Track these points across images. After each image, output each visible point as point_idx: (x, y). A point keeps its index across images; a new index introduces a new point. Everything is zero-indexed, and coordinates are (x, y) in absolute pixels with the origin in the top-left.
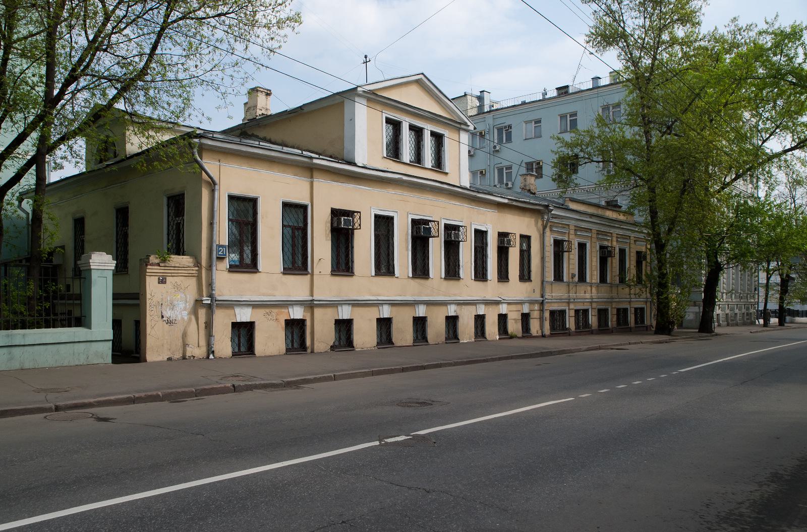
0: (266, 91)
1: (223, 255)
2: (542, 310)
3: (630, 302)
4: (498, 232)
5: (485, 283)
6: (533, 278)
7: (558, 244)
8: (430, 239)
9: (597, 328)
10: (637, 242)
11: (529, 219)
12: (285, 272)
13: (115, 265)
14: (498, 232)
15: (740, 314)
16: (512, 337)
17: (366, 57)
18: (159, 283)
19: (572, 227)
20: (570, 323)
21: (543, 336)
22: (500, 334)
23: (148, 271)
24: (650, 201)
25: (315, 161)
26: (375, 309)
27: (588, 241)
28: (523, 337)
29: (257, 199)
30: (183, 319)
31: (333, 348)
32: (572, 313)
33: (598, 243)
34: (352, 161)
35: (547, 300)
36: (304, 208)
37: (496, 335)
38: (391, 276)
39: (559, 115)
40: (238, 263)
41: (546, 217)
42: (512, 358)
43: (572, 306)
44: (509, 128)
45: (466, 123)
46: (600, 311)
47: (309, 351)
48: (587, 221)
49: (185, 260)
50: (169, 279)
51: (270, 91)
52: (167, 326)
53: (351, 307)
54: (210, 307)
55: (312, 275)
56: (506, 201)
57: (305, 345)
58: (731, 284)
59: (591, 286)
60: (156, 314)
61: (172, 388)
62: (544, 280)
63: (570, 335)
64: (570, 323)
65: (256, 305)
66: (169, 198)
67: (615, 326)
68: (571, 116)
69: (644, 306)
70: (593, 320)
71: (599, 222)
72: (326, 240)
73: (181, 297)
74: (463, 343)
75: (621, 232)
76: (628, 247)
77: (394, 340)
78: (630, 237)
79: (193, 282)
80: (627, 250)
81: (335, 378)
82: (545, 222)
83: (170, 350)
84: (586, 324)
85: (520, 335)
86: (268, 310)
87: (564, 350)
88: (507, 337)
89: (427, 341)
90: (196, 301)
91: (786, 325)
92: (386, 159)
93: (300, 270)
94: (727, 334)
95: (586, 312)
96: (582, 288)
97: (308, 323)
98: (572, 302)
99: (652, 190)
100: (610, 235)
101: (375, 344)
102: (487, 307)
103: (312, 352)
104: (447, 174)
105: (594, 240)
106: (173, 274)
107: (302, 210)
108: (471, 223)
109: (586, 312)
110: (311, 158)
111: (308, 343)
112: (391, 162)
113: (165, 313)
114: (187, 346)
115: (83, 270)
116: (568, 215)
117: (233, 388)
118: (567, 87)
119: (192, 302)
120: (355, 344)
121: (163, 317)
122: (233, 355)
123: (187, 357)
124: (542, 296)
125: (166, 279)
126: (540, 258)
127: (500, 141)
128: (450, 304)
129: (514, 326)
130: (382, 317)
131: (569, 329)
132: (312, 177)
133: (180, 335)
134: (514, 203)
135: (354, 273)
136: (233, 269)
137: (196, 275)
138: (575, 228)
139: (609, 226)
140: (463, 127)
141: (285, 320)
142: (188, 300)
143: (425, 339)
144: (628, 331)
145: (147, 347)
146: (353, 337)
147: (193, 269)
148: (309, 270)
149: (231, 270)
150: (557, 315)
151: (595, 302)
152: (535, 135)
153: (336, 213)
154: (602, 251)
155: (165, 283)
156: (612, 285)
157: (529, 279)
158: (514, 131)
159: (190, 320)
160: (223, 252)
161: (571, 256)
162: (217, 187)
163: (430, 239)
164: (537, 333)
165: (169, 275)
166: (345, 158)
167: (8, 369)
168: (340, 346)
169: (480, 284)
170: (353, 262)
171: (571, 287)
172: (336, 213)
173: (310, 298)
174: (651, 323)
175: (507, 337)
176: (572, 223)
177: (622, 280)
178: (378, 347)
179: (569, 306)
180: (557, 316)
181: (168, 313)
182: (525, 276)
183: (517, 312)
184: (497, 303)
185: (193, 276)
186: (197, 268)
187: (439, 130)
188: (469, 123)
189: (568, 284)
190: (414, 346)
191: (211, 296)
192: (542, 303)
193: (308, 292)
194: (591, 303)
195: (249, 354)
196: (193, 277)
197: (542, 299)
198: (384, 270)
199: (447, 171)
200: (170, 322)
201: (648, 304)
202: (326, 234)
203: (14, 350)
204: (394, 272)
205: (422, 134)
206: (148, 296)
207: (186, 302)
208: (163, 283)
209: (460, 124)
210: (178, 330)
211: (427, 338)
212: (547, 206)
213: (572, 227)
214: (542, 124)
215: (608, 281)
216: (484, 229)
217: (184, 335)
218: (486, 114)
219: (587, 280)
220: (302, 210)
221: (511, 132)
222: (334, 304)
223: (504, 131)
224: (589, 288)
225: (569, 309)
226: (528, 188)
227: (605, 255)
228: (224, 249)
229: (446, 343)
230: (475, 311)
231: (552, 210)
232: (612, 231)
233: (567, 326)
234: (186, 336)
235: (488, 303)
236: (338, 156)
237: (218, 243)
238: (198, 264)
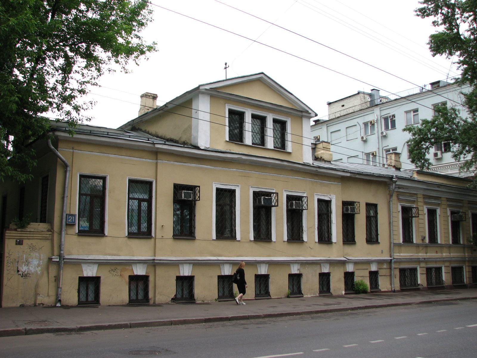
0: (153, 95)
1: (72, 222)
5: (330, 246)
7: (406, 211)
12: (129, 236)
17: (226, 64)
18: (16, 244)
20: (421, 279)
22: (345, 290)
23: (6, 234)
25: (157, 146)
31: (174, 300)
34: (196, 145)
35: (395, 260)
36: (150, 184)
37: (342, 290)
38: (352, 244)
40: (87, 229)
44: (393, 117)
46: (453, 269)
48: (430, 190)
49: (42, 226)
50: (25, 242)
51: (156, 95)
52: (22, 278)
57: (149, 297)
60: (12, 269)
64: (421, 279)
65: (101, 264)
70: (446, 277)
73: (35, 256)
79: (47, 244)
86: (113, 267)
92: (228, 143)
101: (217, 297)
107: (148, 186)
111: (151, 295)
113: (20, 268)
114: (38, 295)
118: (438, 82)
120: (196, 297)
123: (37, 304)
125: (22, 241)
127: (387, 128)
135: (195, 237)
136: (82, 233)
137: (50, 238)
139: (464, 194)
140: (304, 114)
141: (129, 276)
142: (42, 258)
143: (267, 293)
147: (47, 233)
148: (153, 235)
149: (80, 234)
150: (407, 273)
152: (414, 123)
153: (178, 188)
154: (454, 216)
155: (22, 244)
157: (377, 242)
158: (397, 119)
159: (42, 273)
160: (72, 220)
162: (68, 169)
163: (272, 208)
165: (25, 238)
168: (182, 298)
172: (178, 188)
178: (219, 300)
180: (407, 273)
181: (24, 269)
183: (448, 274)
185: (48, 239)
186: (50, 233)
190: (256, 299)
191: (60, 256)
193: (389, 255)
196: (47, 240)
197: (391, 258)
198: (227, 233)
200: (25, 276)
206: (6, 254)
208: (20, 245)
209: (302, 112)
214: (419, 112)
216: (327, 198)
217: (37, 286)
218: (374, 107)
220: (148, 186)
221: (395, 120)
222: (176, 264)
223: (389, 120)
228: (73, 217)
235: (332, 263)
236: (188, 142)
237: (68, 213)
238: (51, 230)
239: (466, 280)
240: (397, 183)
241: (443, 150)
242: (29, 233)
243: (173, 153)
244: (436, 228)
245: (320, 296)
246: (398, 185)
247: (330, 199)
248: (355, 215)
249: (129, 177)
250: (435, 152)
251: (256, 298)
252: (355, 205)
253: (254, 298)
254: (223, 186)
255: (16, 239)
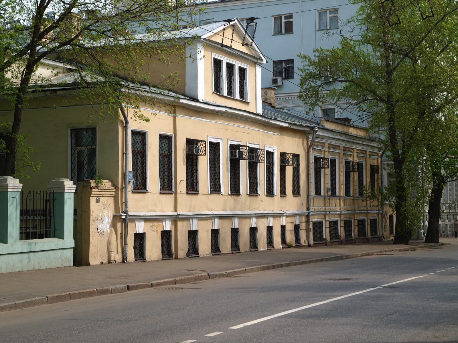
2: (308, 222)
3: (367, 214)
4: (281, 153)
5: (273, 198)
6: (301, 193)
7: (317, 160)
8: (258, 163)
9: (344, 238)
10: (372, 157)
11: (299, 139)
12: (162, 192)
13: (75, 189)
14: (281, 153)
15: (450, 225)
16: (289, 246)
19: (327, 145)
21: (309, 246)
23: (92, 193)
24: (390, 121)
25: (182, 101)
26: (209, 222)
27: (337, 157)
28: (296, 246)
29: (146, 132)
30: (107, 230)
32: (328, 225)
33: (344, 159)
34: (195, 97)
35: (311, 213)
39: (273, 16)
41: (311, 137)
42: (322, 260)
43: (327, 218)
45: (261, 58)
47: (174, 257)
53: (144, 223)
54: (124, 221)
55: (176, 194)
56: (287, 125)
58: (449, 195)
59: (340, 199)
61: (160, 279)
62: (310, 194)
63: (326, 245)
66: (72, 131)
67: (357, 236)
68: (286, 18)
69: (377, 217)
71: (345, 139)
72: (184, 165)
74: (261, 251)
75: (360, 148)
76: (365, 161)
77: (221, 248)
78: (366, 151)
80: (364, 164)
81: (70, 297)
82: (309, 142)
83: (101, 256)
84: (322, 238)
85: (294, 245)
86: (152, 223)
87: (349, 255)
88: (286, 246)
89: (239, 250)
90: (114, 216)
91: (441, 240)
92: (214, 94)
93: (297, 194)
94: (449, 244)
95: (336, 223)
96: (334, 201)
97: (173, 234)
98: (328, 215)
99: (391, 108)
100: (352, 151)
102: (221, 221)
103: (176, 258)
104: (248, 103)
105: (341, 156)
106: (103, 195)
108: (264, 145)
109: (336, 223)
110: (179, 98)
112: (217, 96)
115: (56, 193)
116: (325, 135)
117: (208, 276)
119: (111, 217)
121: (98, 230)
122: (135, 260)
123: (112, 262)
124: (308, 209)
126: (306, 174)
128: (253, 217)
129: (290, 237)
130: (214, 229)
131: (326, 239)
132: (175, 112)
133: (105, 244)
134: (292, 127)
137: (114, 195)
138: (329, 146)
144: (366, 241)
145: (90, 254)
146: (198, 245)
148: (173, 190)
151: (344, 214)
156: (354, 198)
159: (111, 231)
161: (327, 171)
164: (305, 243)
165: (101, 195)
166: (187, 93)
167: (28, 270)
169: (269, 199)
170: (197, 182)
171: (326, 200)
173: (175, 213)
174: (383, 234)
175: (286, 246)
176: (327, 141)
177: (361, 194)
178: (213, 254)
179: (325, 218)
182: (296, 192)
184: (280, 215)
187: (244, 66)
188: (263, 58)
189: (325, 196)
190: (232, 253)
191: (126, 212)
192: (308, 216)
193: (172, 208)
194: (340, 215)
195: (141, 260)
196: (112, 197)
197: (308, 212)
199: (249, 101)
201: (380, 215)
202: (183, 159)
203: (32, 255)
204: (220, 191)
205: (233, 70)
206: (91, 213)
207: (109, 217)
209: (257, 59)
210: (105, 238)
211: (239, 246)
212: (312, 128)
213: (327, 145)
215: (351, 194)
216: (272, 151)
217: (109, 244)
219: (337, 194)
224: (338, 201)
225: (325, 221)
226: (269, 102)
227: (349, 168)
229: (251, 251)
230: (267, 223)
231: (317, 131)
232: (354, 146)
233: (324, 237)
234: (110, 244)
239: (354, 234)
240: (317, 133)
241: (284, 76)
242: (104, 190)
243: (184, 107)
244: (195, 167)
245: (251, 251)
246: (317, 135)
247: (273, 151)
248: (199, 156)
249: (315, 154)
250: (274, 78)
251: (233, 252)
252: (199, 144)
253: (231, 252)
254: (213, 139)
255: (95, 198)
